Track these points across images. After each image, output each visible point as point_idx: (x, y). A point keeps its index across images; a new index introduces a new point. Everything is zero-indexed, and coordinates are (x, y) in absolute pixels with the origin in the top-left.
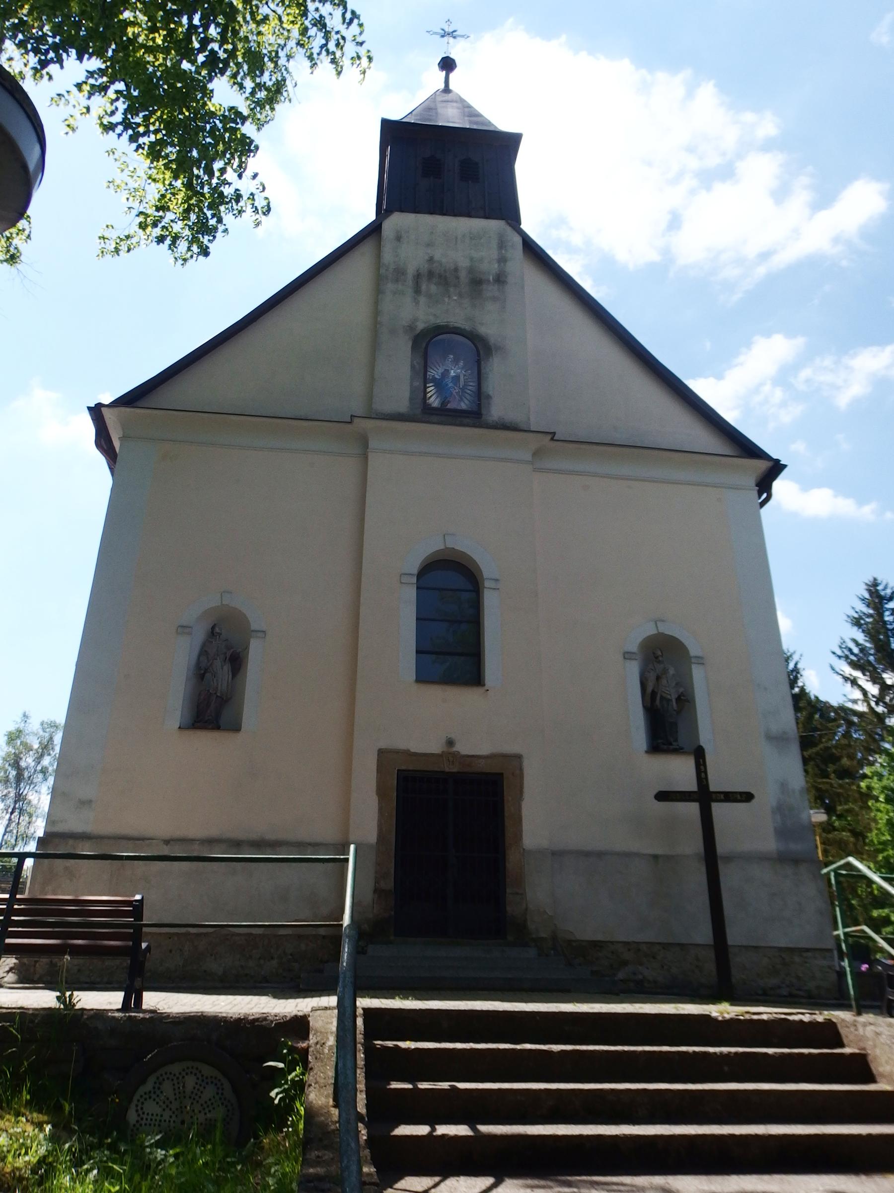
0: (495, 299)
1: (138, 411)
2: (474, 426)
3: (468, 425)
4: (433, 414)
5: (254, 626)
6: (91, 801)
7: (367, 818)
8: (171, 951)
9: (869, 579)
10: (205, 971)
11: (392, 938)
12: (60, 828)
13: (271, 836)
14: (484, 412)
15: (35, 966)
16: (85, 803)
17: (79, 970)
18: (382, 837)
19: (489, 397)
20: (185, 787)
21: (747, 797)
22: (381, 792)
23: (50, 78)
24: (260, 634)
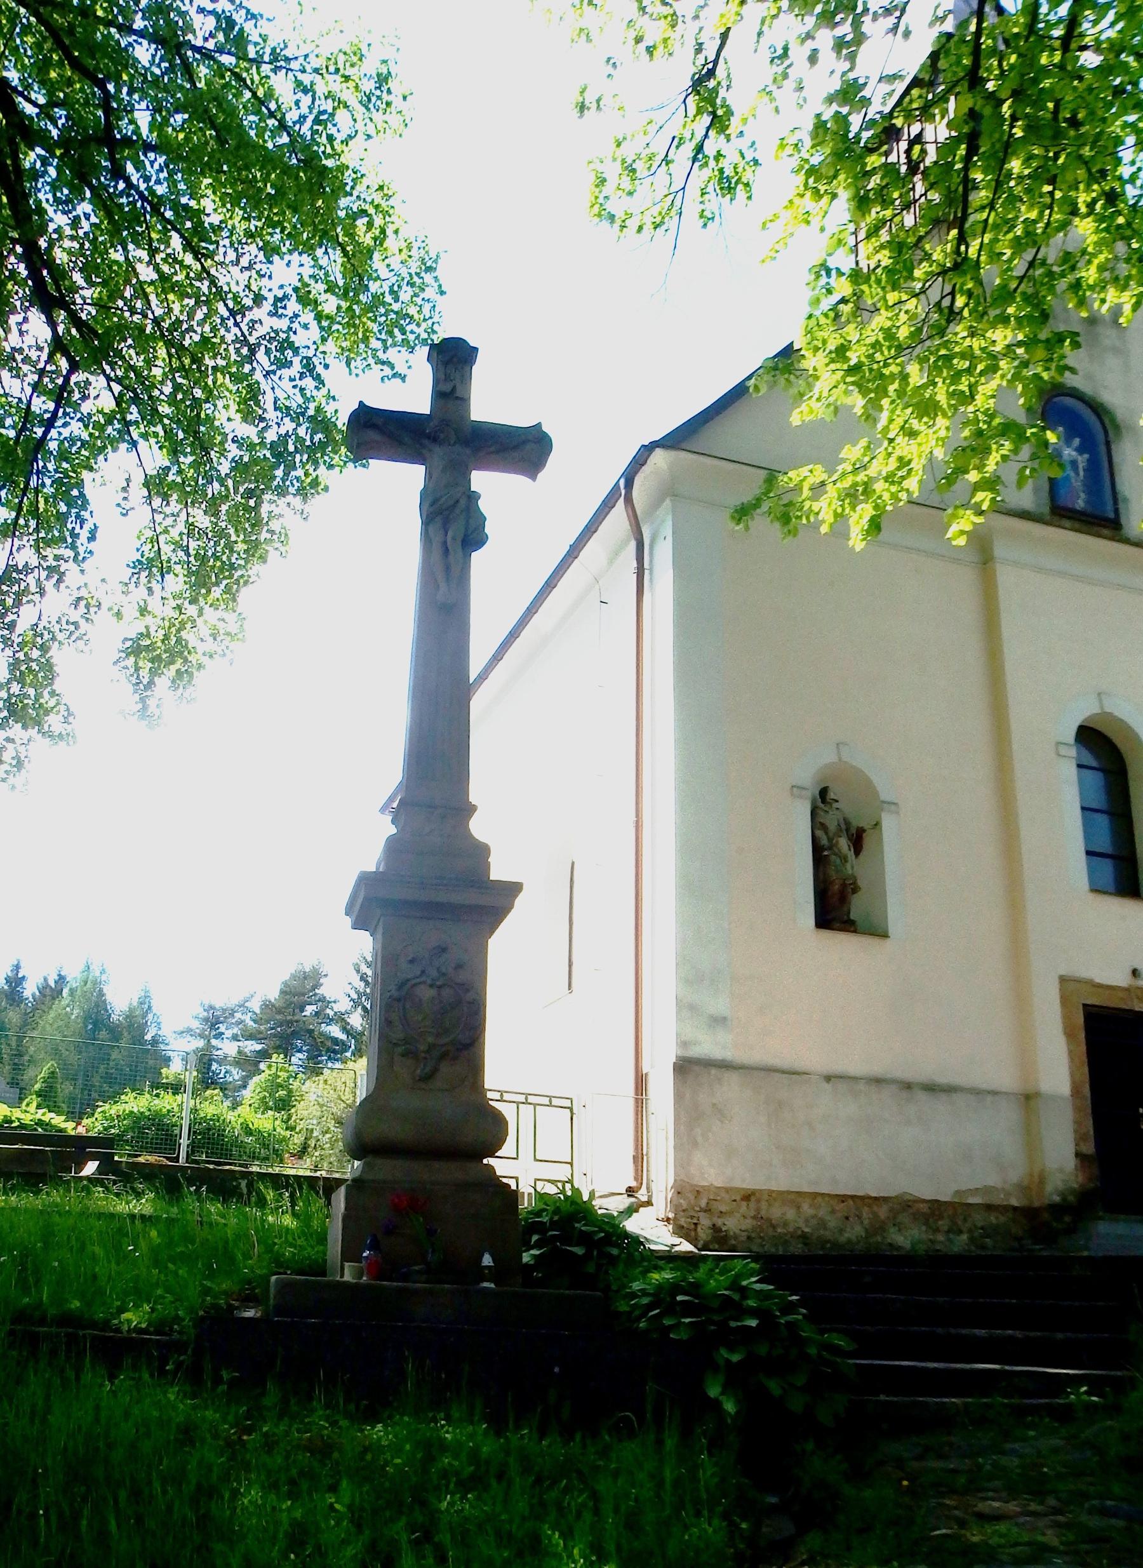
0: (1116, 351)
1: (683, 454)
2: (1112, 539)
3: (1105, 538)
4: (1064, 517)
5: (884, 796)
6: (725, 1019)
7: (1057, 1068)
8: (847, 1218)
9: (807, 775)
10: (890, 1245)
11: (1101, 1214)
12: (695, 1052)
13: (942, 1080)
14: (1123, 521)
15: (695, 1230)
16: (718, 1021)
17: (749, 1238)
18: (1076, 1091)
19: (1126, 500)
20: (829, 1006)
21: (573, 864)
22: (1069, 1034)
23: (128, 566)
24: (893, 807)
